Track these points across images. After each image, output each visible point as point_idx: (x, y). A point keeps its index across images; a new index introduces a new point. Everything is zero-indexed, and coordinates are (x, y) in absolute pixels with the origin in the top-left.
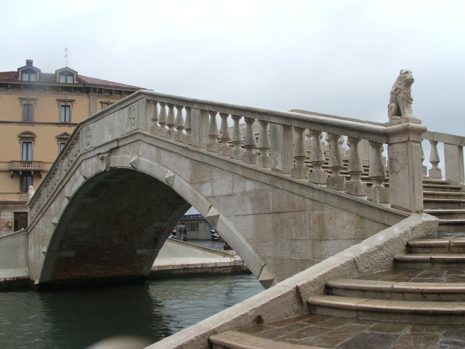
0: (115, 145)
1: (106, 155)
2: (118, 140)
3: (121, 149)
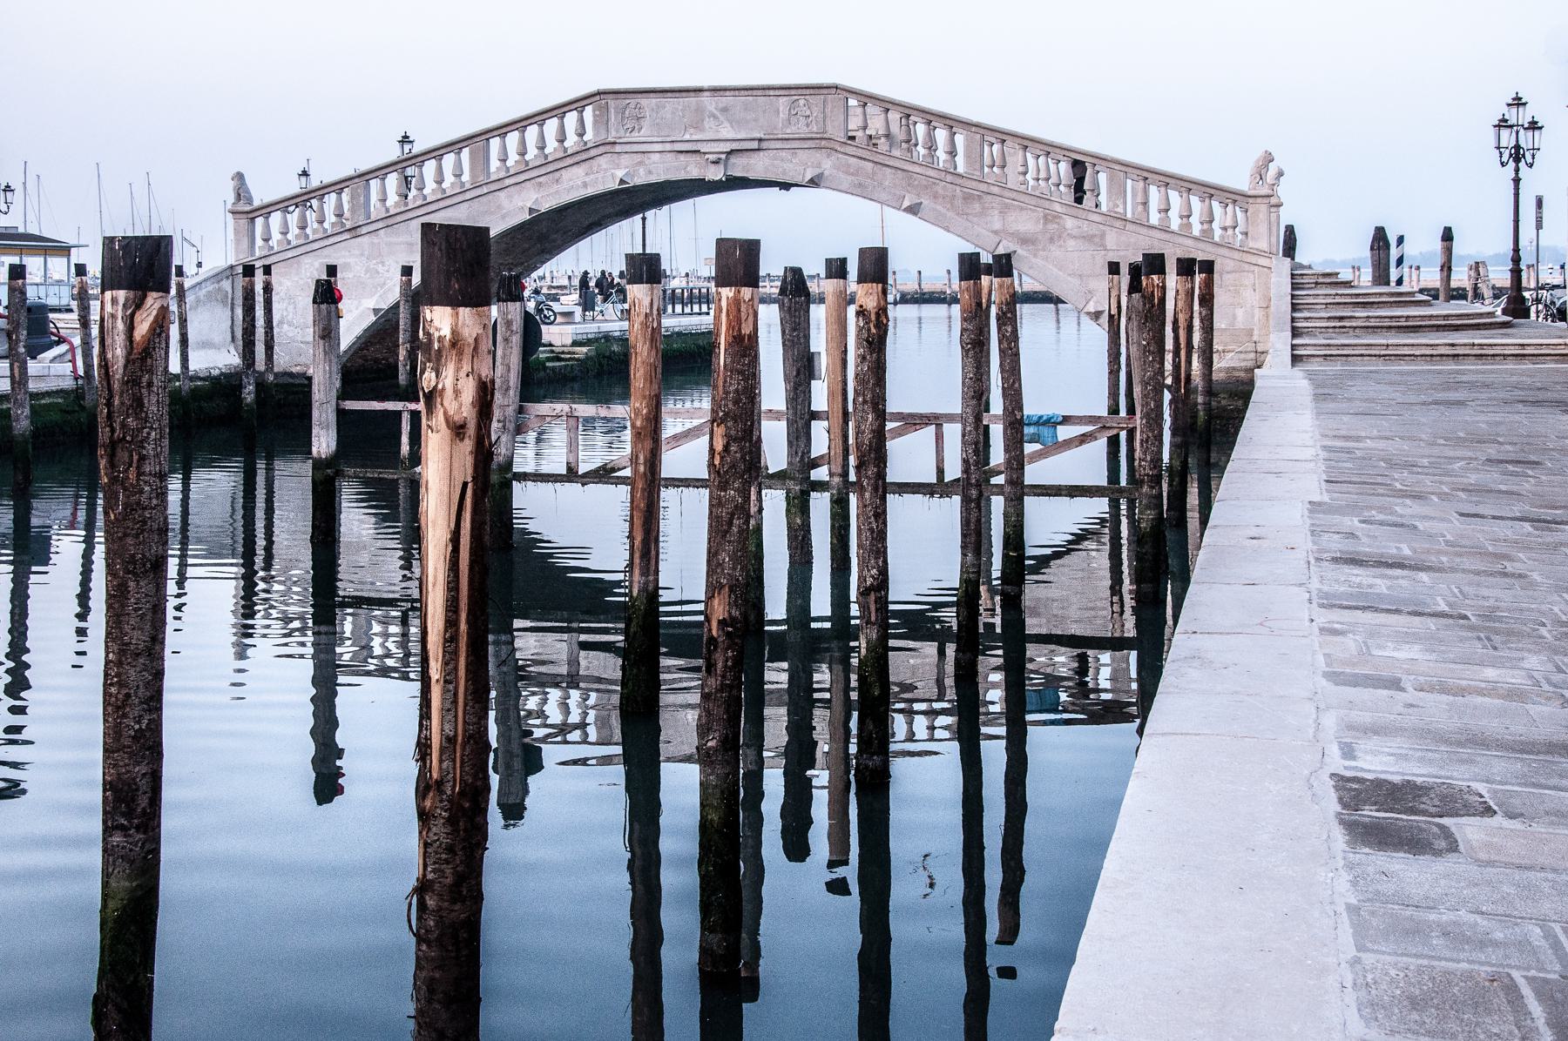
0: (755, 145)
1: (723, 156)
2: (760, 140)
3: (761, 153)
